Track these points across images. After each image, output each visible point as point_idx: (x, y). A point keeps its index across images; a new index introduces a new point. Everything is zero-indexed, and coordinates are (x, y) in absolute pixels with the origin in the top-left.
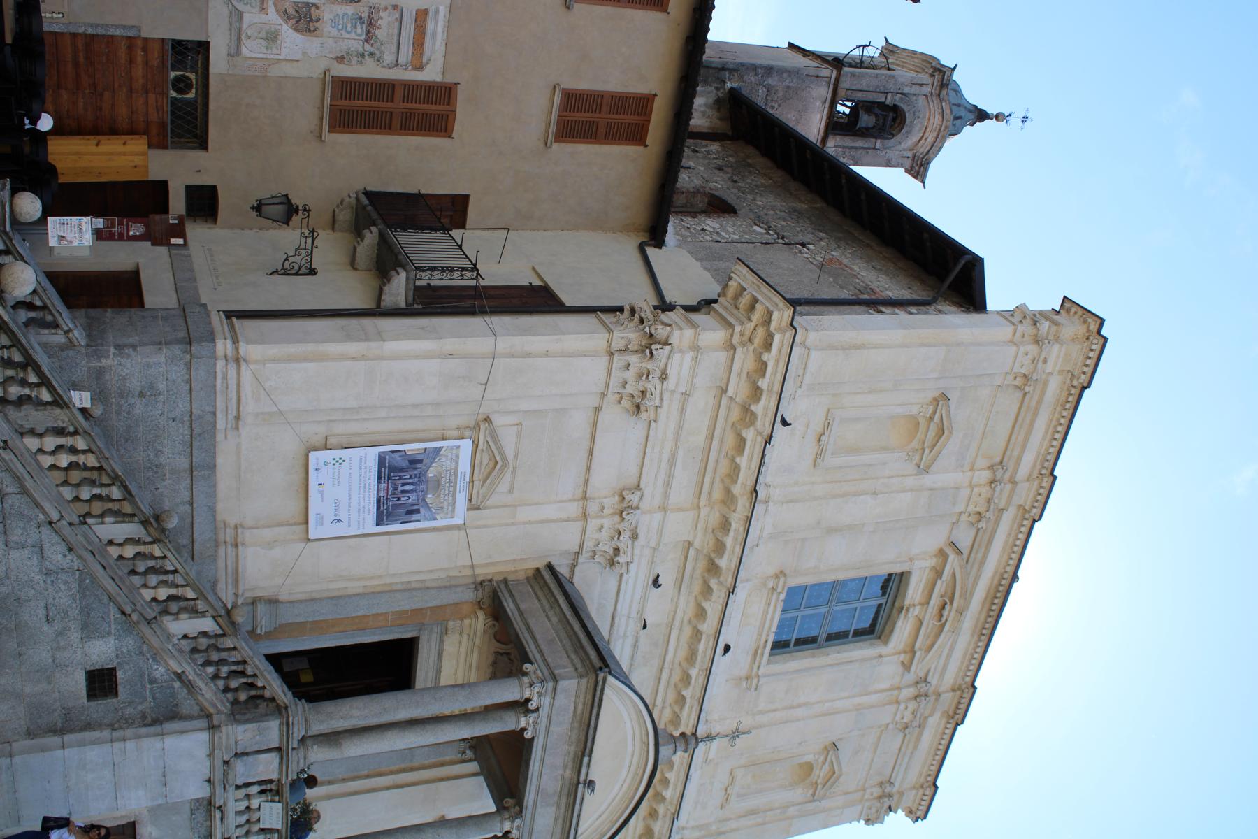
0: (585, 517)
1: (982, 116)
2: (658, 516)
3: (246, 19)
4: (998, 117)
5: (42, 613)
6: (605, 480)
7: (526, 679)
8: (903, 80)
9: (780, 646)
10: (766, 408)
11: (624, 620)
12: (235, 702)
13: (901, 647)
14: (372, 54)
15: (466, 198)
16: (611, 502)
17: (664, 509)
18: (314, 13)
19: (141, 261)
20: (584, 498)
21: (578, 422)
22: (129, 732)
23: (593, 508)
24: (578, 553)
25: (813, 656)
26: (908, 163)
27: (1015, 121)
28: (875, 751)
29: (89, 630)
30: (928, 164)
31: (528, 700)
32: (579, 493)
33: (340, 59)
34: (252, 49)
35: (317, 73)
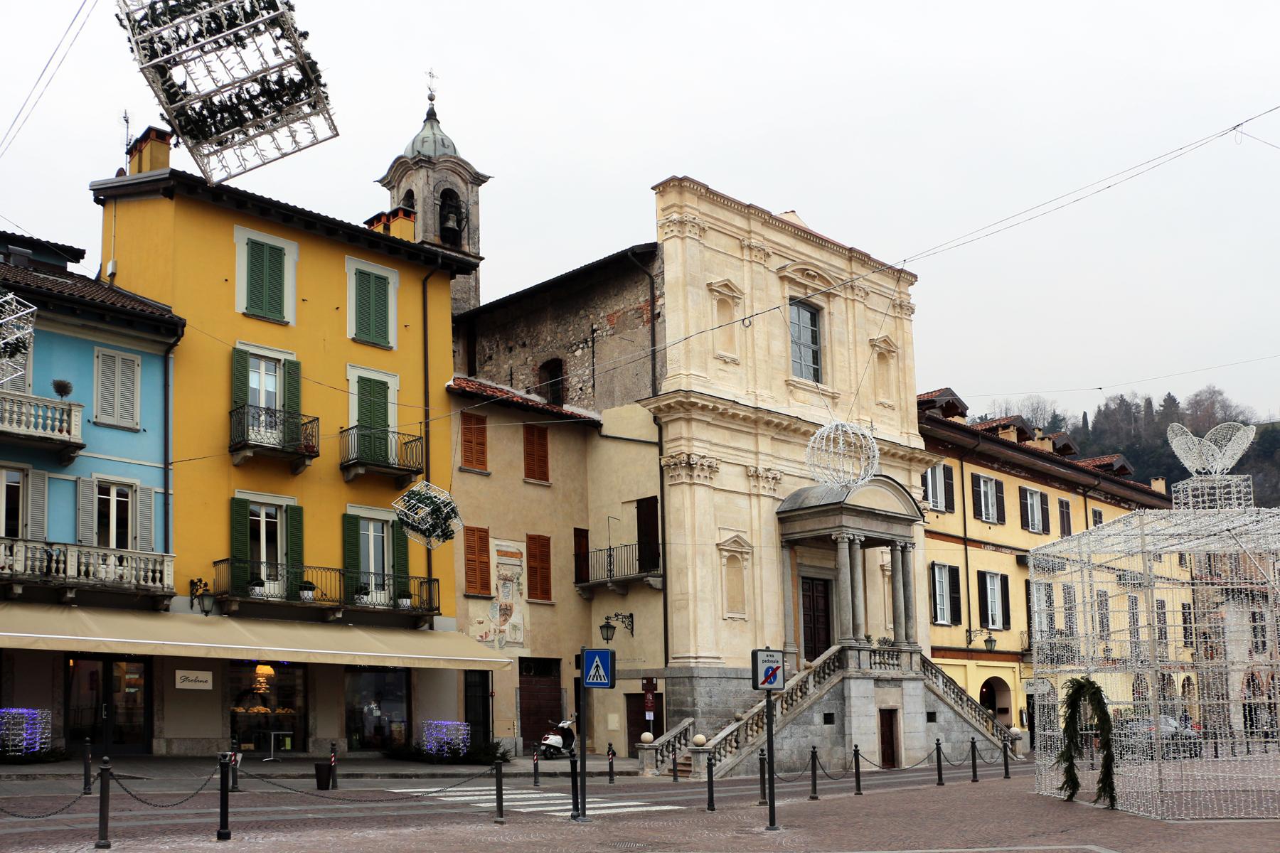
0: (758, 496)
1: (431, 116)
2: (761, 457)
3: (508, 640)
4: (431, 98)
5: (804, 739)
6: (742, 485)
7: (839, 540)
8: (426, 192)
9: (817, 377)
10: (721, 404)
11: (803, 472)
12: (839, 668)
13: (825, 299)
14: (518, 579)
15: (576, 530)
16: (753, 483)
17: (757, 453)
18: (503, 607)
19: (622, 692)
20: (749, 495)
21: (719, 497)
22: (847, 710)
23: (754, 491)
24: (774, 498)
25: (825, 355)
26: (475, 188)
27: (435, 85)
28: (876, 311)
29: (810, 722)
30: (477, 173)
31: (849, 539)
32: (747, 497)
33: (521, 594)
34: (520, 637)
35: (527, 606)
